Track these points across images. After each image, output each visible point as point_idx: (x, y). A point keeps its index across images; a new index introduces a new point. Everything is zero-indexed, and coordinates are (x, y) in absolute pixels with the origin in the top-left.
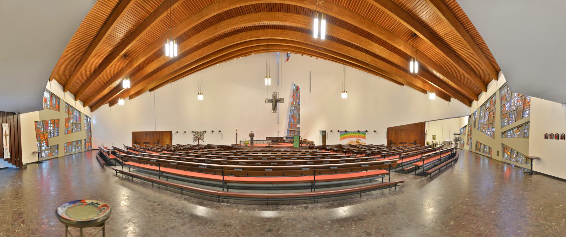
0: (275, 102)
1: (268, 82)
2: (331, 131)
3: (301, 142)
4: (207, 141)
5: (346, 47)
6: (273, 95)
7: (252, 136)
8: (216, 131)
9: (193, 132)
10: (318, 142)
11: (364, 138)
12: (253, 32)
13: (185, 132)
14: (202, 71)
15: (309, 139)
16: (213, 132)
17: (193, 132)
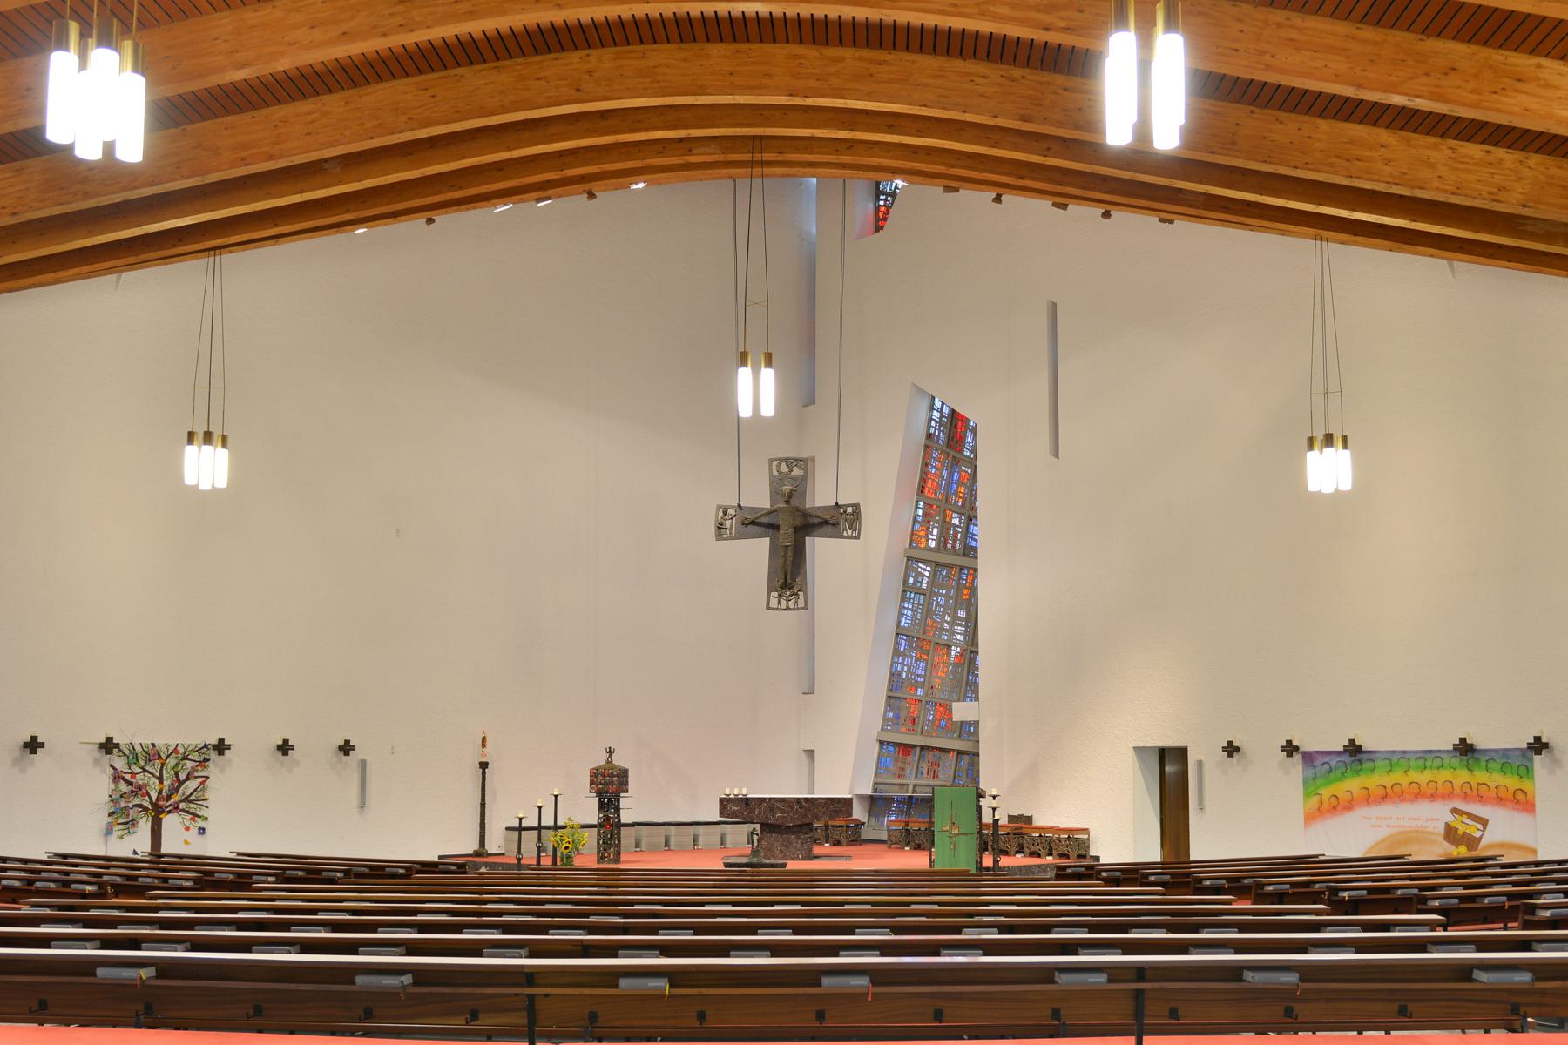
0: (792, 529)
1: (757, 392)
2: (1231, 749)
3: (991, 839)
4: (238, 821)
5: (1325, 130)
6: (776, 483)
7: (609, 785)
8: (315, 745)
9: (108, 746)
10: (1124, 835)
11: (1523, 803)
12: (663, 56)
13: (33, 745)
14: (227, 258)
15: (1052, 815)
16: (285, 748)
17: (108, 746)
